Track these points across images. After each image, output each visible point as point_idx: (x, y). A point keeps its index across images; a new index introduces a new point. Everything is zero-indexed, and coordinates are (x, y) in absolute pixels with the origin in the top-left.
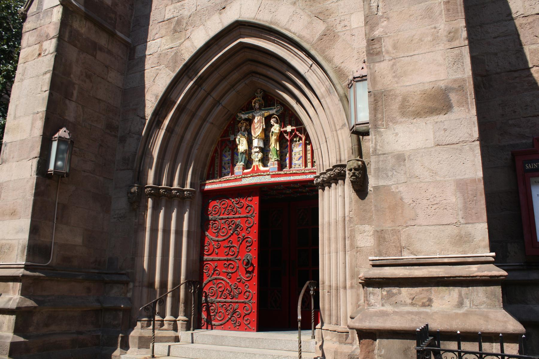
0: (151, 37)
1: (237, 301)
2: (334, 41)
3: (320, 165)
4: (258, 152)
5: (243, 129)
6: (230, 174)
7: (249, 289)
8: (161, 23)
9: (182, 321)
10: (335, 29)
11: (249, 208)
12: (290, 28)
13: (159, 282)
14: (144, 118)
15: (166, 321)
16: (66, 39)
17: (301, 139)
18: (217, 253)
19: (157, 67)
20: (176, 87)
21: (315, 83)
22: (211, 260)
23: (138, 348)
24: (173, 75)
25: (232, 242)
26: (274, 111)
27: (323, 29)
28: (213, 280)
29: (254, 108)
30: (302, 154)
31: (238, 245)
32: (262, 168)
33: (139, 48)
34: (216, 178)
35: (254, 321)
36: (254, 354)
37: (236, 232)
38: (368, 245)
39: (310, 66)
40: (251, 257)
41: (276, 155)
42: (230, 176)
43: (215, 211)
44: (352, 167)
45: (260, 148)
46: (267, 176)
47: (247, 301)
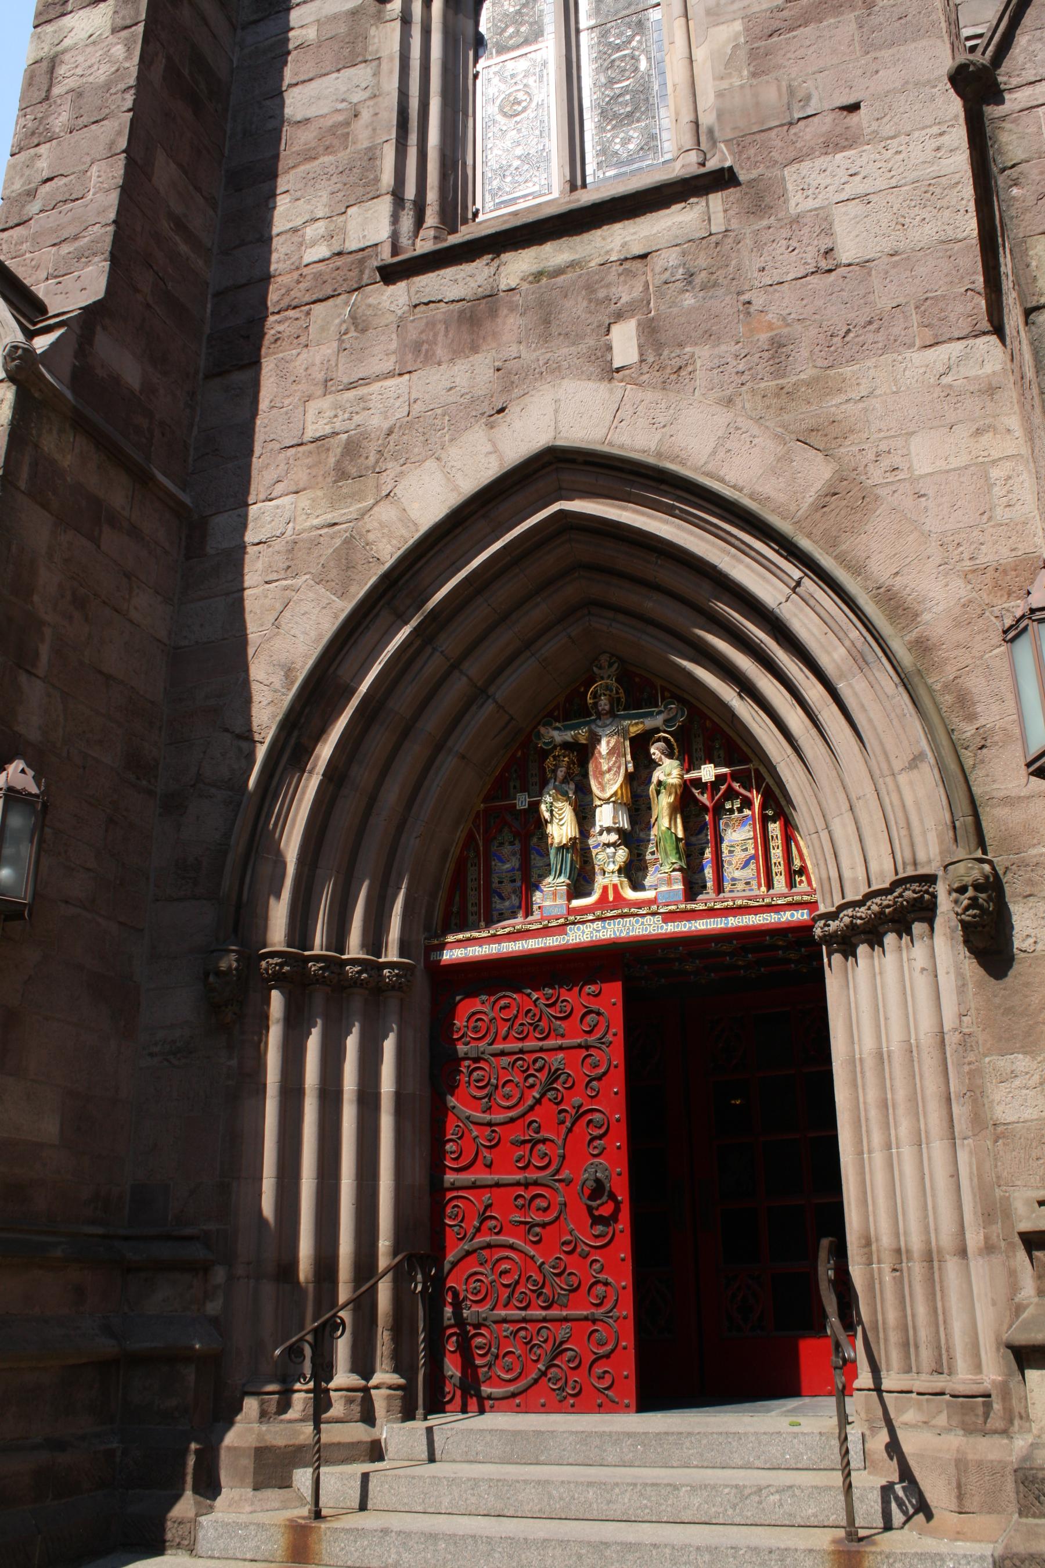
0: (262, 489)
1: (564, 1313)
2: (864, 512)
3: (829, 878)
4: (614, 845)
5: (561, 773)
6: (521, 914)
7: (606, 1274)
8: (293, 450)
9: (390, 1388)
10: (863, 477)
11: (591, 1018)
12: (722, 473)
13: (311, 1261)
14: (247, 737)
15: (336, 1390)
16: (23, 485)
17: (747, 803)
18: (489, 1163)
19: (284, 583)
20: (355, 641)
21: (813, 634)
22: (470, 1184)
23: (255, 1489)
24: (345, 607)
25: (540, 1127)
26: (658, 721)
27: (827, 475)
28: (482, 1248)
29: (593, 712)
30: (756, 848)
31: (558, 1136)
32: (629, 894)
33: (220, 521)
34: (476, 927)
35: (626, 1377)
36: (670, 1485)
37: (551, 1095)
38: (1029, 1117)
39: (794, 584)
40: (607, 1173)
41: (674, 852)
42: (520, 919)
43: (476, 1030)
44: (968, 880)
45: (619, 831)
46: (648, 917)
47: (599, 1312)
